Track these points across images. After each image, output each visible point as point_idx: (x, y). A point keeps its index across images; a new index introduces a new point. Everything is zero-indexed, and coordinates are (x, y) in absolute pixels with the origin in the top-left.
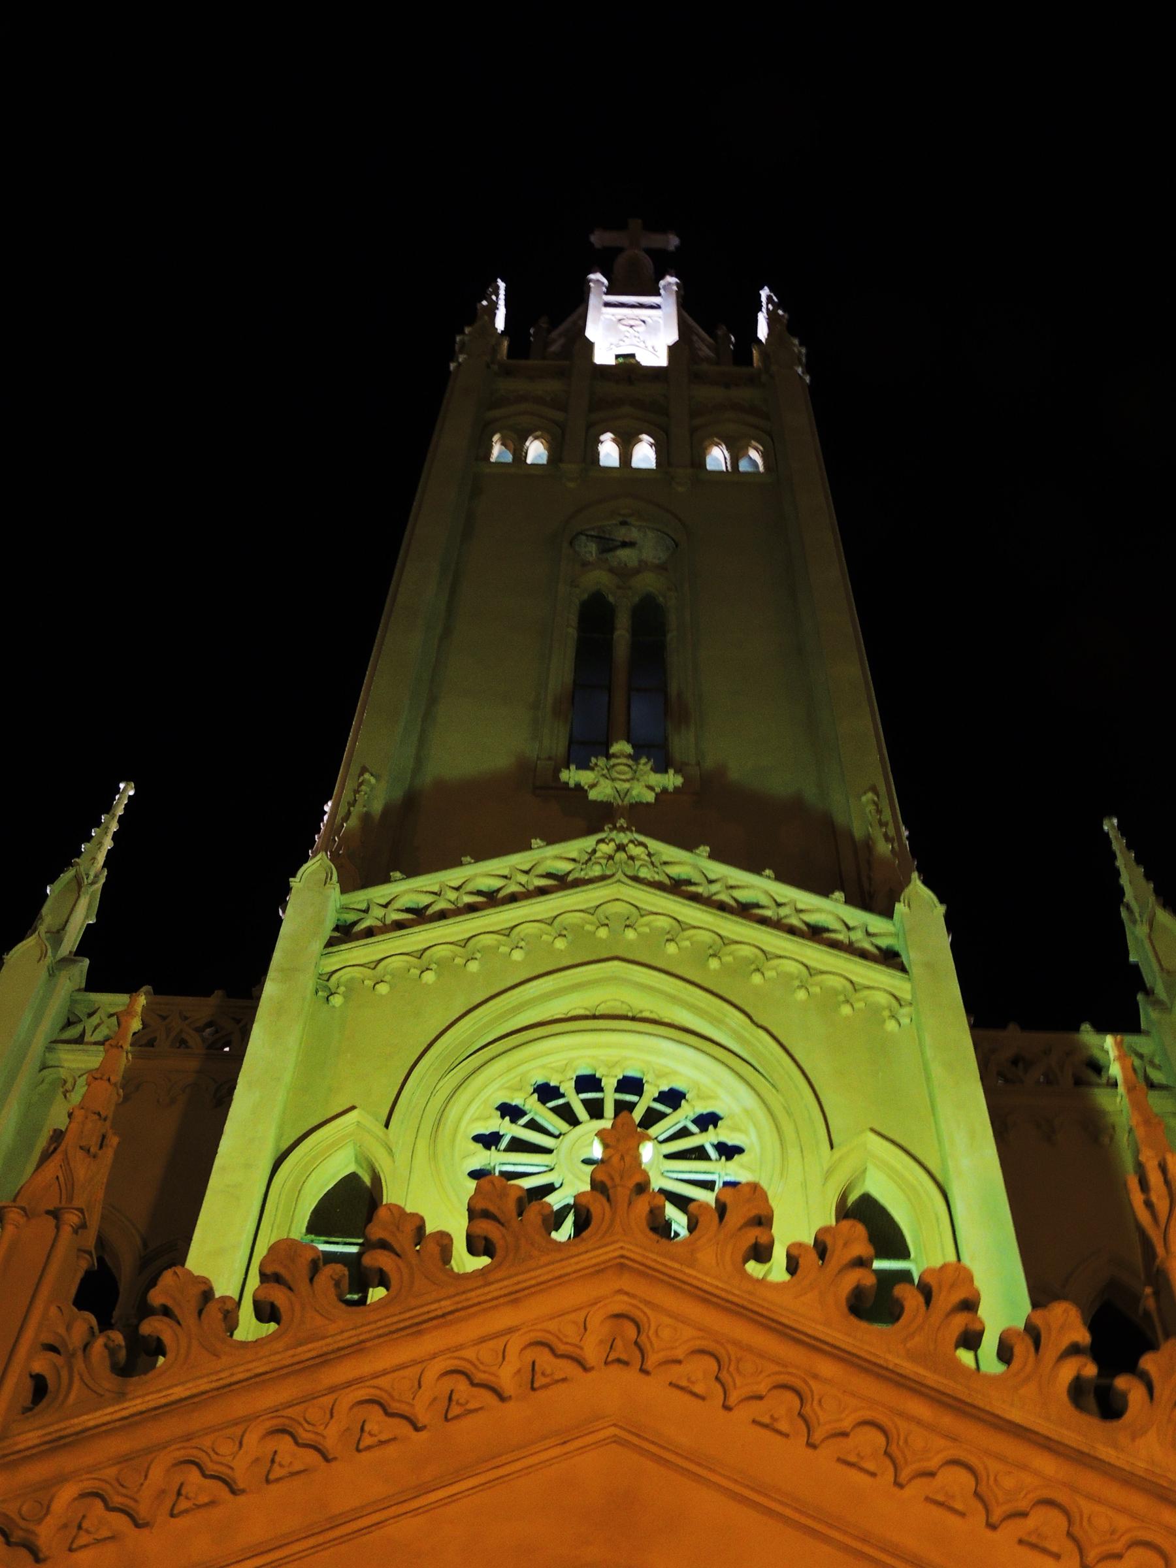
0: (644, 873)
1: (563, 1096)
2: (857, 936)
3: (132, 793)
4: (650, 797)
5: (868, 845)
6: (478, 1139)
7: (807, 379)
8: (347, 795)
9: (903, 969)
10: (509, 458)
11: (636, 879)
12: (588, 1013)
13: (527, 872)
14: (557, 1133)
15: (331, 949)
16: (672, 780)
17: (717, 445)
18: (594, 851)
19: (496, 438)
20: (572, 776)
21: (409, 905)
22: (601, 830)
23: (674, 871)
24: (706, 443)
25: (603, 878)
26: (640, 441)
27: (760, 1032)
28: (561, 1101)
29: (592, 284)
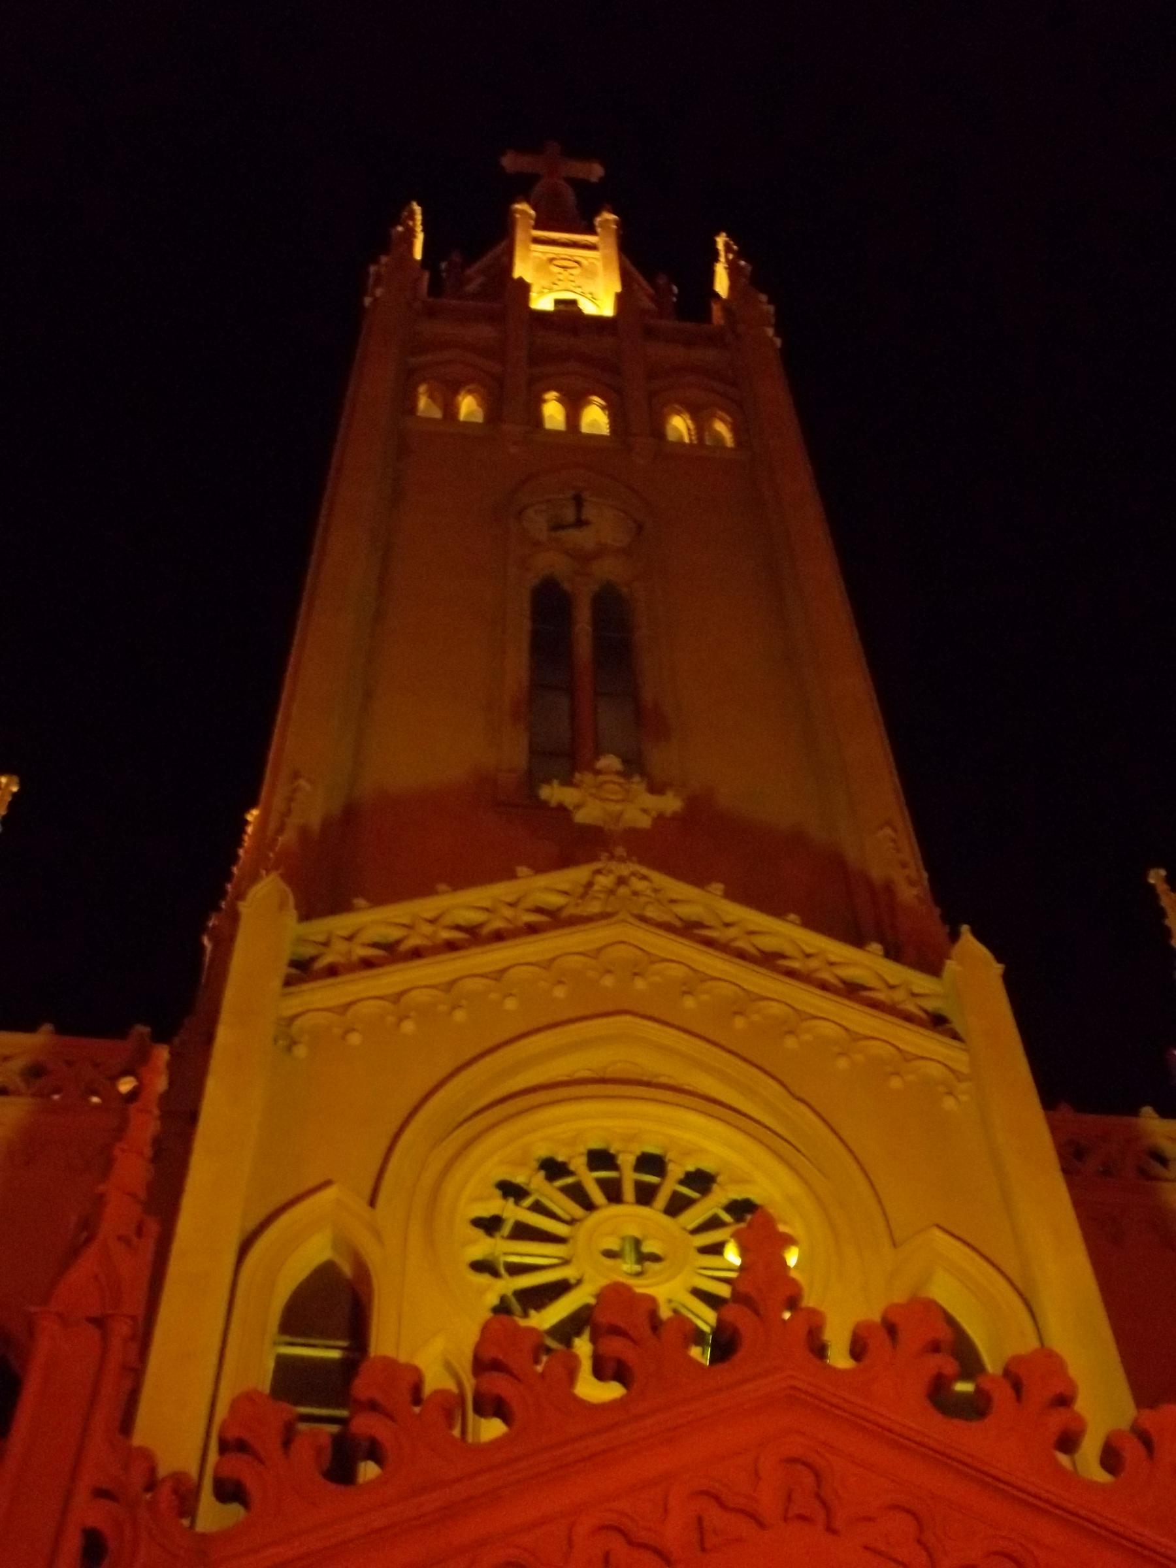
0: (650, 912)
1: (571, 1173)
2: (899, 996)
3: (15, 789)
4: (645, 822)
5: (889, 888)
6: (478, 1223)
7: (778, 342)
8: (278, 803)
9: (955, 1036)
10: (437, 414)
11: (643, 919)
12: (594, 1075)
13: (511, 905)
14: (567, 1217)
15: (293, 989)
16: (671, 803)
17: (679, 413)
18: (590, 885)
19: (422, 389)
20: (554, 793)
21: (376, 939)
22: (595, 858)
23: (685, 911)
24: (666, 410)
25: (605, 916)
26: (589, 403)
27: (803, 1108)
28: (570, 1180)
29: (518, 216)
